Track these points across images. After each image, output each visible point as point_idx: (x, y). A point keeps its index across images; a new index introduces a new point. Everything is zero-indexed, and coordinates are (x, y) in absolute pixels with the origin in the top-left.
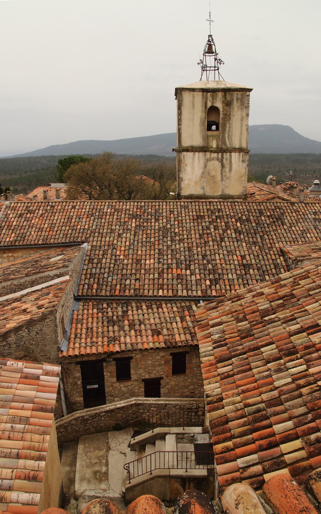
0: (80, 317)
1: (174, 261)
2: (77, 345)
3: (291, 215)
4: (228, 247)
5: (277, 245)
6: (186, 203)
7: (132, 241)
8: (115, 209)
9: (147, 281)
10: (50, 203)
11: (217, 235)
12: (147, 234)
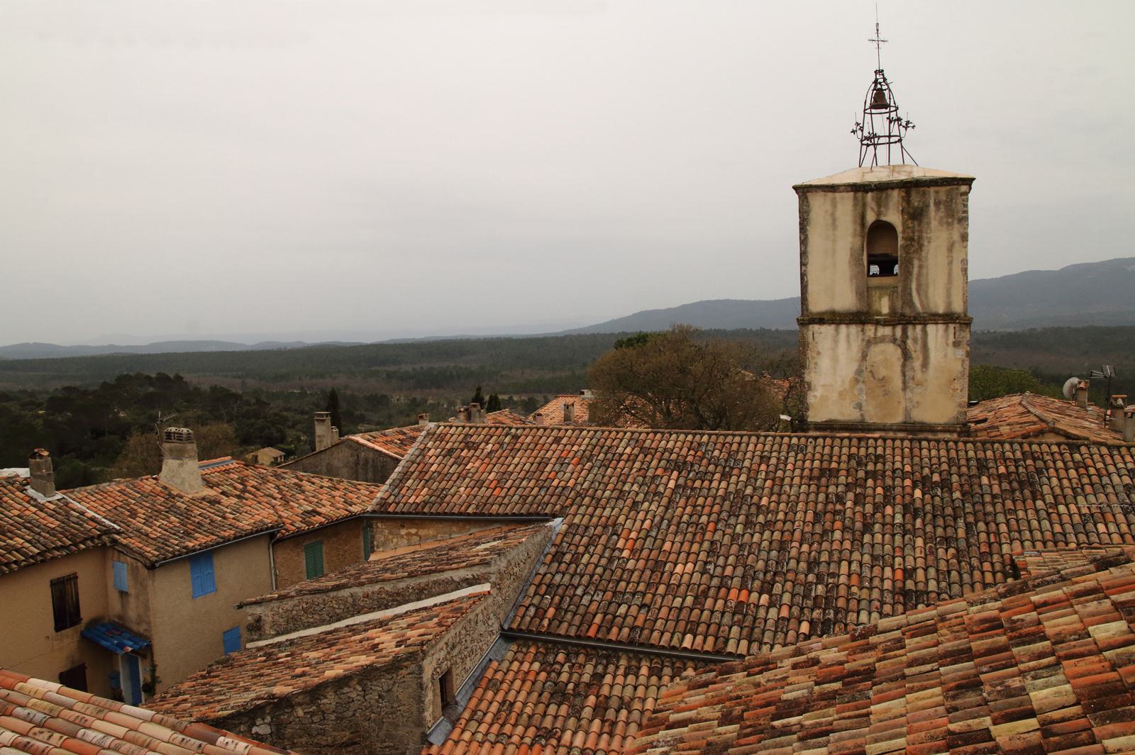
0: (499, 676)
1: (740, 571)
2: (467, 736)
3: (1063, 474)
4: (878, 547)
5: (1006, 548)
6: (803, 440)
7: (657, 519)
8: (641, 448)
9: (664, 611)
10: (513, 431)
11: (858, 517)
12: (695, 506)
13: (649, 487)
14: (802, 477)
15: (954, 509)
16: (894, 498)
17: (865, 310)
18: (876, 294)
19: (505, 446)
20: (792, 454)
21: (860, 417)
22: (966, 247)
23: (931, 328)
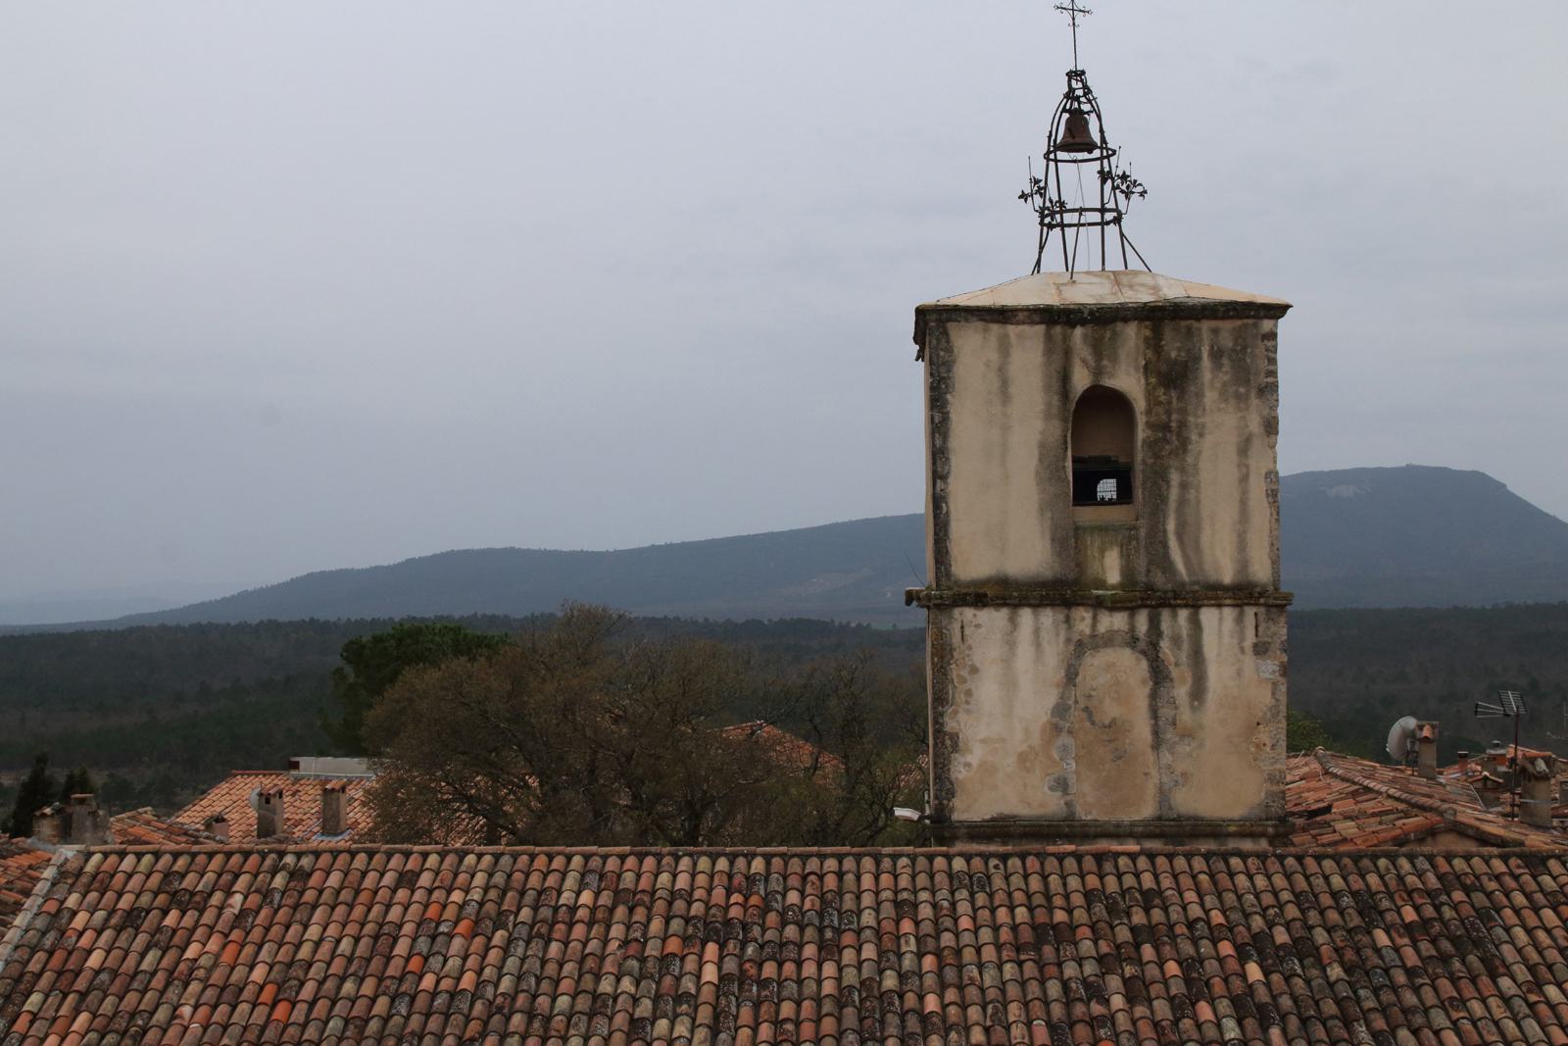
3: (1532, 920)
6: (977, 862)
10: (289, 859)
13: (658, 983)
14: (999, 947)
15: (1338, 1002)
16: (1207, 983)
17: (1071, 576)
18: (1093, 543)
19: (277, 897)
20: (963, 894)
21: (1065, 808)
22: (1273, 447)
23: (1208, 616)
